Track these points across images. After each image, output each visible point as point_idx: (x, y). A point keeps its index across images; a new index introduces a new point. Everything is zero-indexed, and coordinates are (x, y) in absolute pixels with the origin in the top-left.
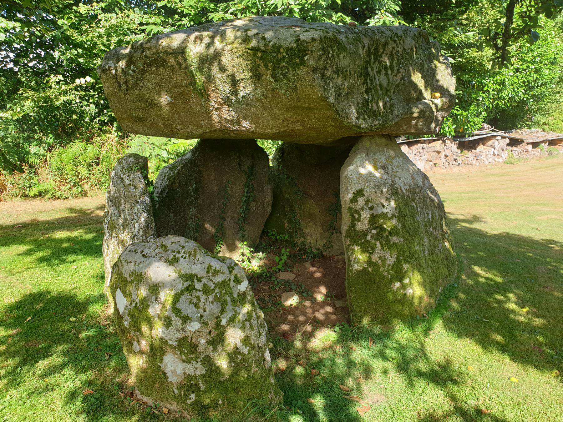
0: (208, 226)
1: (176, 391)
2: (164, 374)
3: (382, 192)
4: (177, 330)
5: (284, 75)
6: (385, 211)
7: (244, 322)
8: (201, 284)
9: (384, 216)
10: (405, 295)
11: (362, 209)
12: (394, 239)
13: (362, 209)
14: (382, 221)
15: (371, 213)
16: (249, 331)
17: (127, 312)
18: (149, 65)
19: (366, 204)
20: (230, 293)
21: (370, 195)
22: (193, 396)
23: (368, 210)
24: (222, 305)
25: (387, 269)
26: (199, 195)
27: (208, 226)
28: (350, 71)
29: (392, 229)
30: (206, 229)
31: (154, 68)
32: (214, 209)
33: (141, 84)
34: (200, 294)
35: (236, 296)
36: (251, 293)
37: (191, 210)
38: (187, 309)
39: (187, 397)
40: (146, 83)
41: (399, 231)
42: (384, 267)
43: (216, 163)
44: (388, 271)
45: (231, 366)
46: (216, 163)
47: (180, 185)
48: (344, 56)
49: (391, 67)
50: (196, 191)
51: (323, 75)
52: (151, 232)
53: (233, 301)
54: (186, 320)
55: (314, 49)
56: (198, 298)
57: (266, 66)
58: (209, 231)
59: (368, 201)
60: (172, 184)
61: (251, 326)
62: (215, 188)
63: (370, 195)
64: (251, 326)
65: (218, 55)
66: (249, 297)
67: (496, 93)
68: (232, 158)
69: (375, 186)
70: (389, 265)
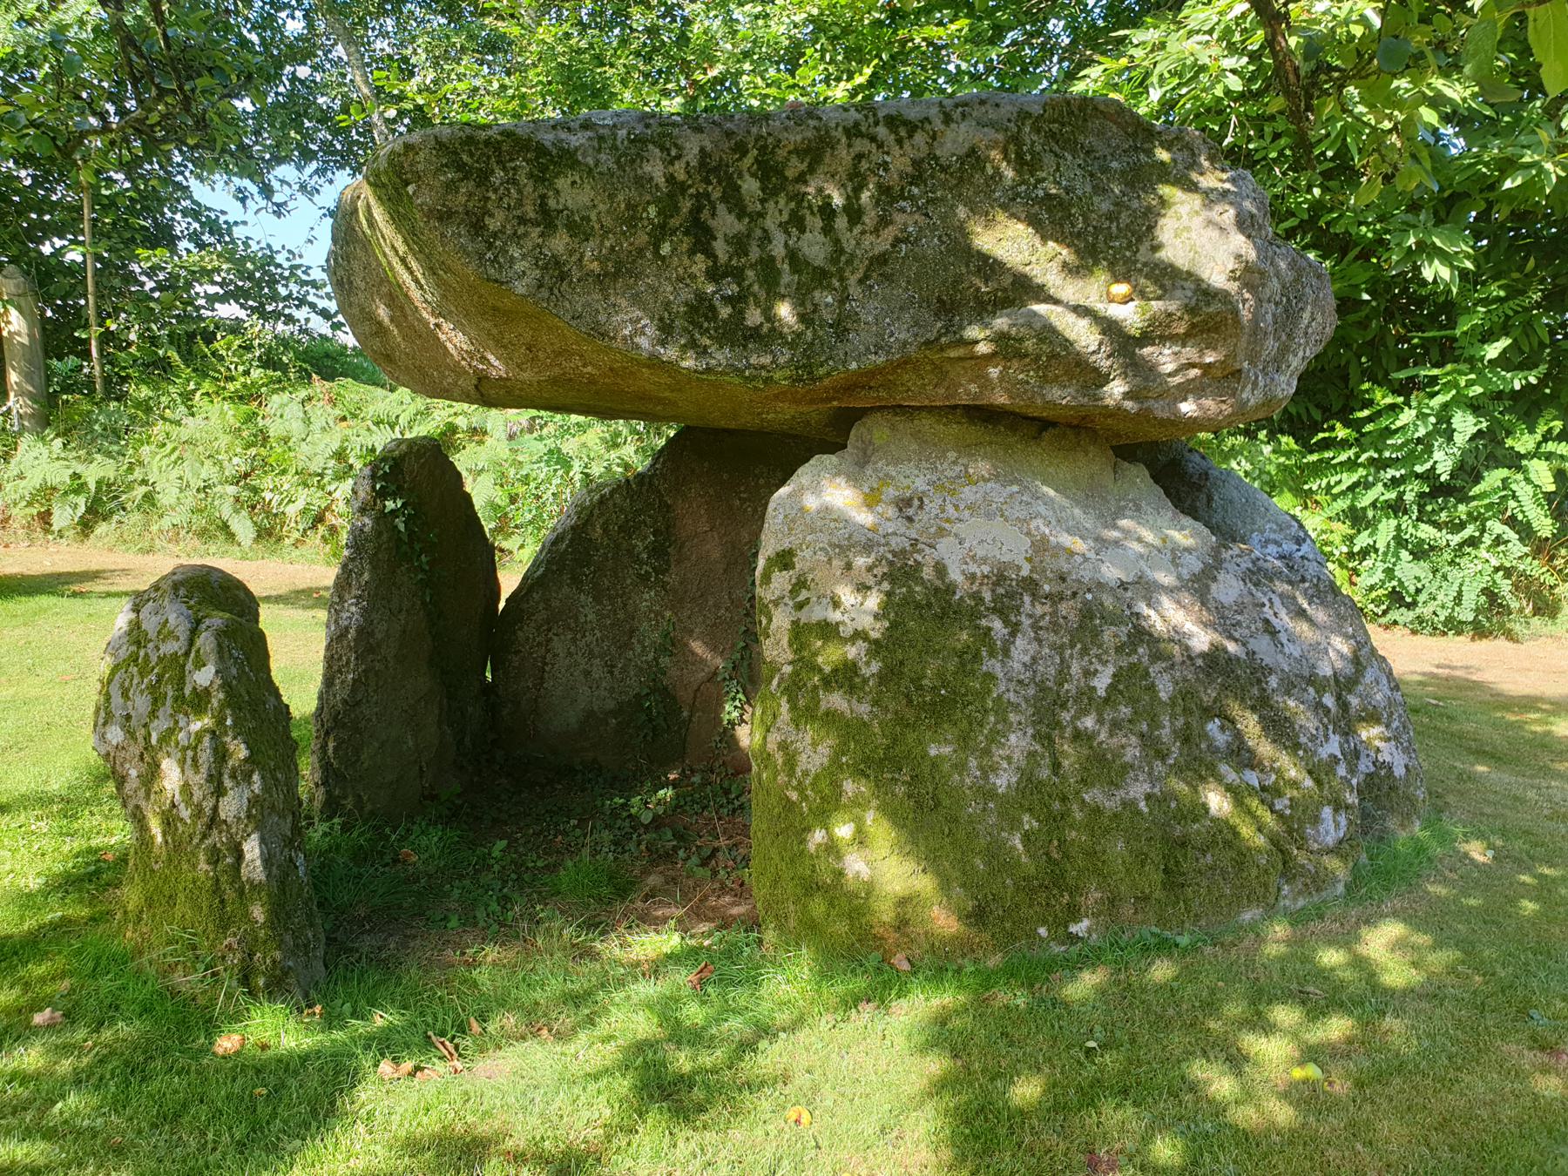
0: (698, 647)
3: (849, 566)
6: (836, 616)
7: (185, 749)
9: (828, 631)
10: (840, 874)
11: (776, 603)
12: (836, 700)
13: (776, 603)
14: (819, 643)
15: (795, 615)
16: (190, 772)
19: (794, 592)
20: (181, 682)
21: (812, 570)
23: (789, 609)
24: (155, 700)
25: (800, 783)
26: (668, 562)
27: (698, 647)
28: (599, 221)
29: (835, 671)
30: (693, 653)
32: (717, 606)
35: (187, 691)
36: (221, 696)
37: (646, 596)
41: (865, 681)
42: (791, 773)
43: (711, 491)
44: (800, 788)
46: (711, 491)
47: (605, 530)
48: (574, 183)
49: (854, 213)
50: (658, 551)
51: (477, 227)
52: (355, 592)
53: (179, 698)
55: (420, 167)
58: (703, 661)
59: (800, 584)
60: (584, 525)
61: (195, 760)
62: (716, 554)
63: (812, 570)
64: (195, 760)
66: (215, 702)
68: (762, 481)
69: (830, 545)
70: (806, 773)
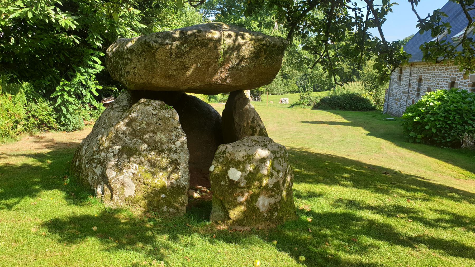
1: (265, 215)
2: (258, 208)
4: (276, 178)
5: (271, 58)
8: (279, 154)
17: (243, 178)
18: (197, 45)
22: (276, 213)
31: (199, 47)
33: (186, 55)
34: (280, 159)
38: (279, 167)
39: (272, 215)
40: (189, 55)
45: (419, 143)
54: (278, 172)
56: (280, 161)
57: (265, 53)
65: (240, 46)
67: (383, 68)
